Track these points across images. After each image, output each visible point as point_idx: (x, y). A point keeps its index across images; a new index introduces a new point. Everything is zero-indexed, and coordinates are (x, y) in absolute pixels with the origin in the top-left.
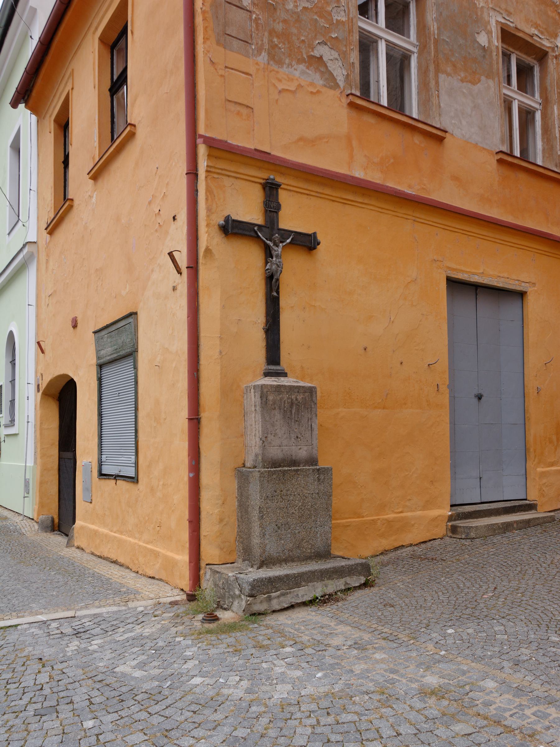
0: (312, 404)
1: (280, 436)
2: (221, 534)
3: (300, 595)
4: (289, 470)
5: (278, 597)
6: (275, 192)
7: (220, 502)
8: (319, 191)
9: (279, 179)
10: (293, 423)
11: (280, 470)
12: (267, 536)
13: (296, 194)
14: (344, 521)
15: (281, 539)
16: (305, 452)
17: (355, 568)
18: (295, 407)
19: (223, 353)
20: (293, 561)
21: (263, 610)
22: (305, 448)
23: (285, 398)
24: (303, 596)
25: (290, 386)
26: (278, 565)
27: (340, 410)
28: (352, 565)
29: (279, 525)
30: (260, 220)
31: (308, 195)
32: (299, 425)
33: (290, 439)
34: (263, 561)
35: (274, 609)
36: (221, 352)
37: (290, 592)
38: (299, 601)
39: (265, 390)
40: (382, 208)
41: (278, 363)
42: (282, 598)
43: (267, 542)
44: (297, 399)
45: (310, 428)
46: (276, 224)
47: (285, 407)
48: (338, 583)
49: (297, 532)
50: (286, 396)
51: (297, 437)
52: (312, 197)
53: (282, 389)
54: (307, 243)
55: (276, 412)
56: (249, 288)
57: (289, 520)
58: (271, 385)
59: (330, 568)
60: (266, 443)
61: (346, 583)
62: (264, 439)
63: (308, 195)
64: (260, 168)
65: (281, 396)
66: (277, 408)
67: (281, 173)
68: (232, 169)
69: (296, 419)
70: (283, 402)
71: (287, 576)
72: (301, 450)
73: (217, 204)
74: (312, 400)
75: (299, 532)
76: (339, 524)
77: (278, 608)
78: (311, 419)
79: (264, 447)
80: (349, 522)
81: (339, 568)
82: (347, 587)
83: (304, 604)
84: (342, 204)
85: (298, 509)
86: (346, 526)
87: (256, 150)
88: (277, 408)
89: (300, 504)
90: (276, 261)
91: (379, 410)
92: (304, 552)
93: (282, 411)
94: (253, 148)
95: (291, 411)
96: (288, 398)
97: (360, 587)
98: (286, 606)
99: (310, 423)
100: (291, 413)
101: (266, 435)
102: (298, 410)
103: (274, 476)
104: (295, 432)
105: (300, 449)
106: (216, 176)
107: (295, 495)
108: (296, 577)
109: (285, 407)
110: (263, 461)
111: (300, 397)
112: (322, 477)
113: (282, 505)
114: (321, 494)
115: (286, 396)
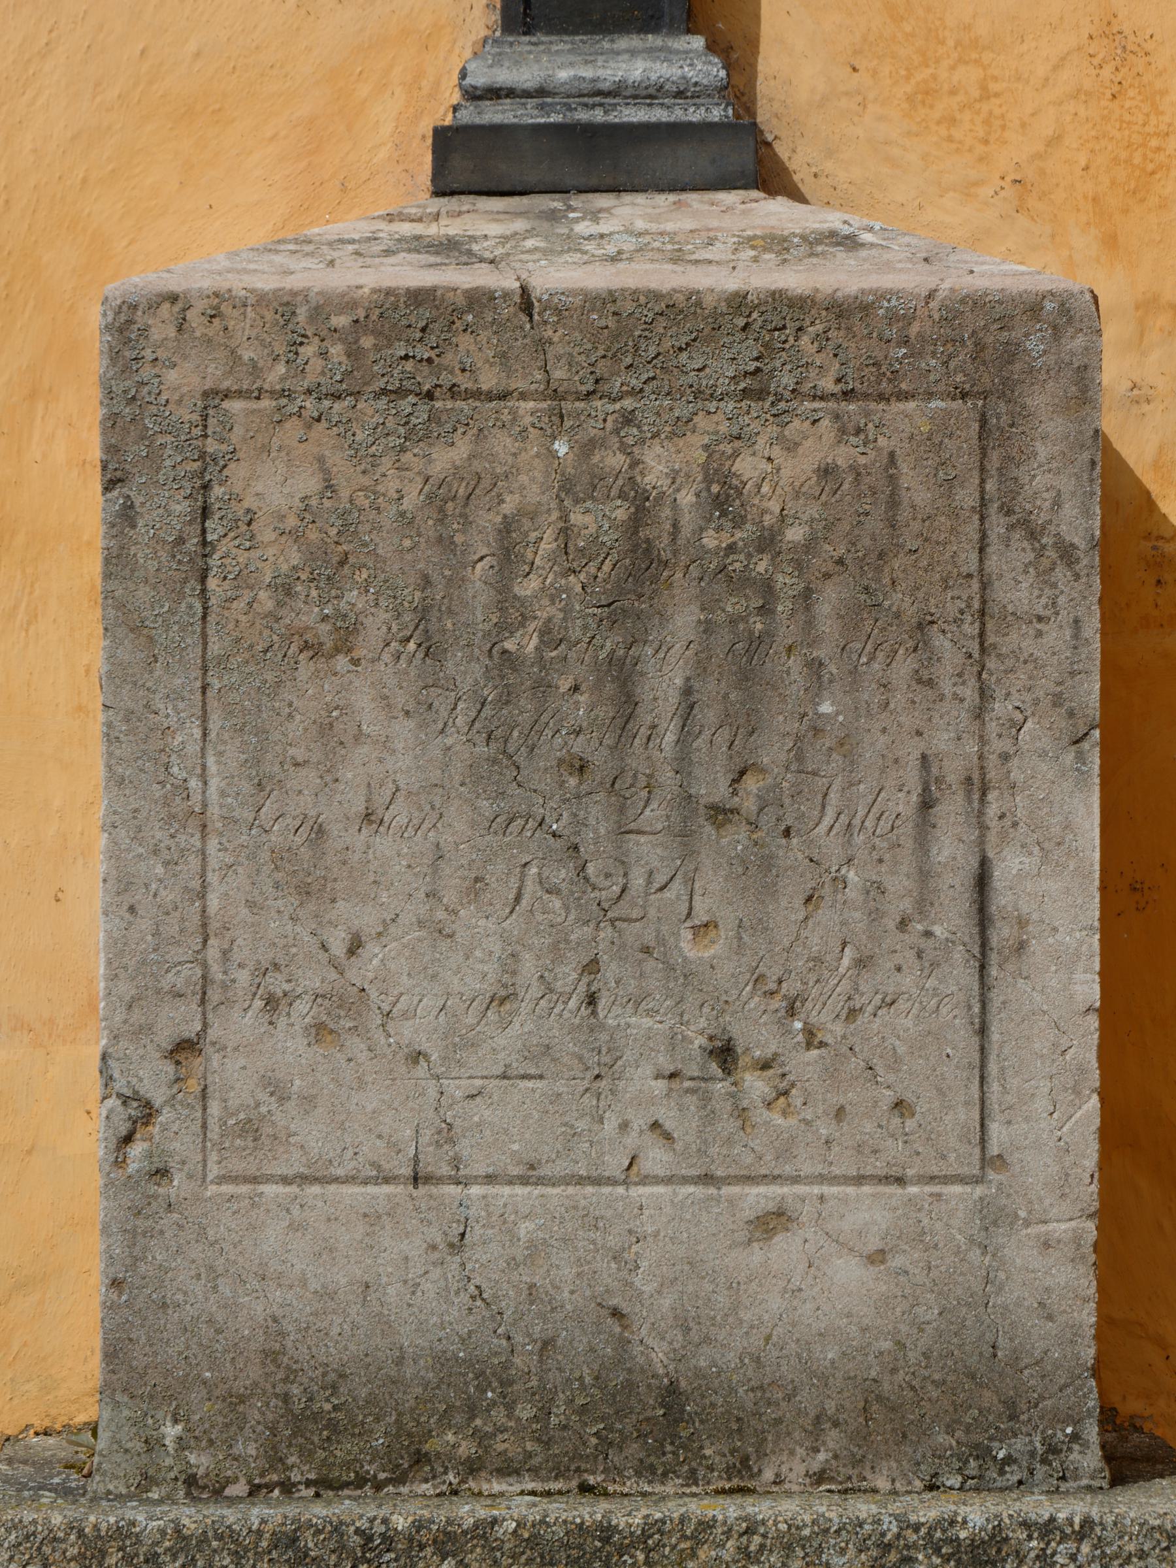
10: (650, 853)
16: (848, 1272)
18: (684, 619)
22: (869, 1212)
23: (530, 489)
25: (610, 298)
32: (758, 872)
33: (603, 1073)
39: (183, 380)
44: (724, 499)
45: (951, 919)
47: (509, 612)
50: (526, 462)
51: (724, 1053)
53: (476, 357)
55: (370, 690)
60: (174, 1133)
62: (152, 1077)
65: (445, 458)
69: (712, 786)
70: (481, 542)
72: (786, 1250)
78: (978, 786)
93: (466, 670)
95: (622, 677)
96: (569, 489)
99: (951, 849)
100: (627, 705)
101: (181, 1019)
102: (746, 661)
104: (688, 975)
105: (774, 1221)
109: (509, 612)
110: (125, 1365)
111: (782, 465)
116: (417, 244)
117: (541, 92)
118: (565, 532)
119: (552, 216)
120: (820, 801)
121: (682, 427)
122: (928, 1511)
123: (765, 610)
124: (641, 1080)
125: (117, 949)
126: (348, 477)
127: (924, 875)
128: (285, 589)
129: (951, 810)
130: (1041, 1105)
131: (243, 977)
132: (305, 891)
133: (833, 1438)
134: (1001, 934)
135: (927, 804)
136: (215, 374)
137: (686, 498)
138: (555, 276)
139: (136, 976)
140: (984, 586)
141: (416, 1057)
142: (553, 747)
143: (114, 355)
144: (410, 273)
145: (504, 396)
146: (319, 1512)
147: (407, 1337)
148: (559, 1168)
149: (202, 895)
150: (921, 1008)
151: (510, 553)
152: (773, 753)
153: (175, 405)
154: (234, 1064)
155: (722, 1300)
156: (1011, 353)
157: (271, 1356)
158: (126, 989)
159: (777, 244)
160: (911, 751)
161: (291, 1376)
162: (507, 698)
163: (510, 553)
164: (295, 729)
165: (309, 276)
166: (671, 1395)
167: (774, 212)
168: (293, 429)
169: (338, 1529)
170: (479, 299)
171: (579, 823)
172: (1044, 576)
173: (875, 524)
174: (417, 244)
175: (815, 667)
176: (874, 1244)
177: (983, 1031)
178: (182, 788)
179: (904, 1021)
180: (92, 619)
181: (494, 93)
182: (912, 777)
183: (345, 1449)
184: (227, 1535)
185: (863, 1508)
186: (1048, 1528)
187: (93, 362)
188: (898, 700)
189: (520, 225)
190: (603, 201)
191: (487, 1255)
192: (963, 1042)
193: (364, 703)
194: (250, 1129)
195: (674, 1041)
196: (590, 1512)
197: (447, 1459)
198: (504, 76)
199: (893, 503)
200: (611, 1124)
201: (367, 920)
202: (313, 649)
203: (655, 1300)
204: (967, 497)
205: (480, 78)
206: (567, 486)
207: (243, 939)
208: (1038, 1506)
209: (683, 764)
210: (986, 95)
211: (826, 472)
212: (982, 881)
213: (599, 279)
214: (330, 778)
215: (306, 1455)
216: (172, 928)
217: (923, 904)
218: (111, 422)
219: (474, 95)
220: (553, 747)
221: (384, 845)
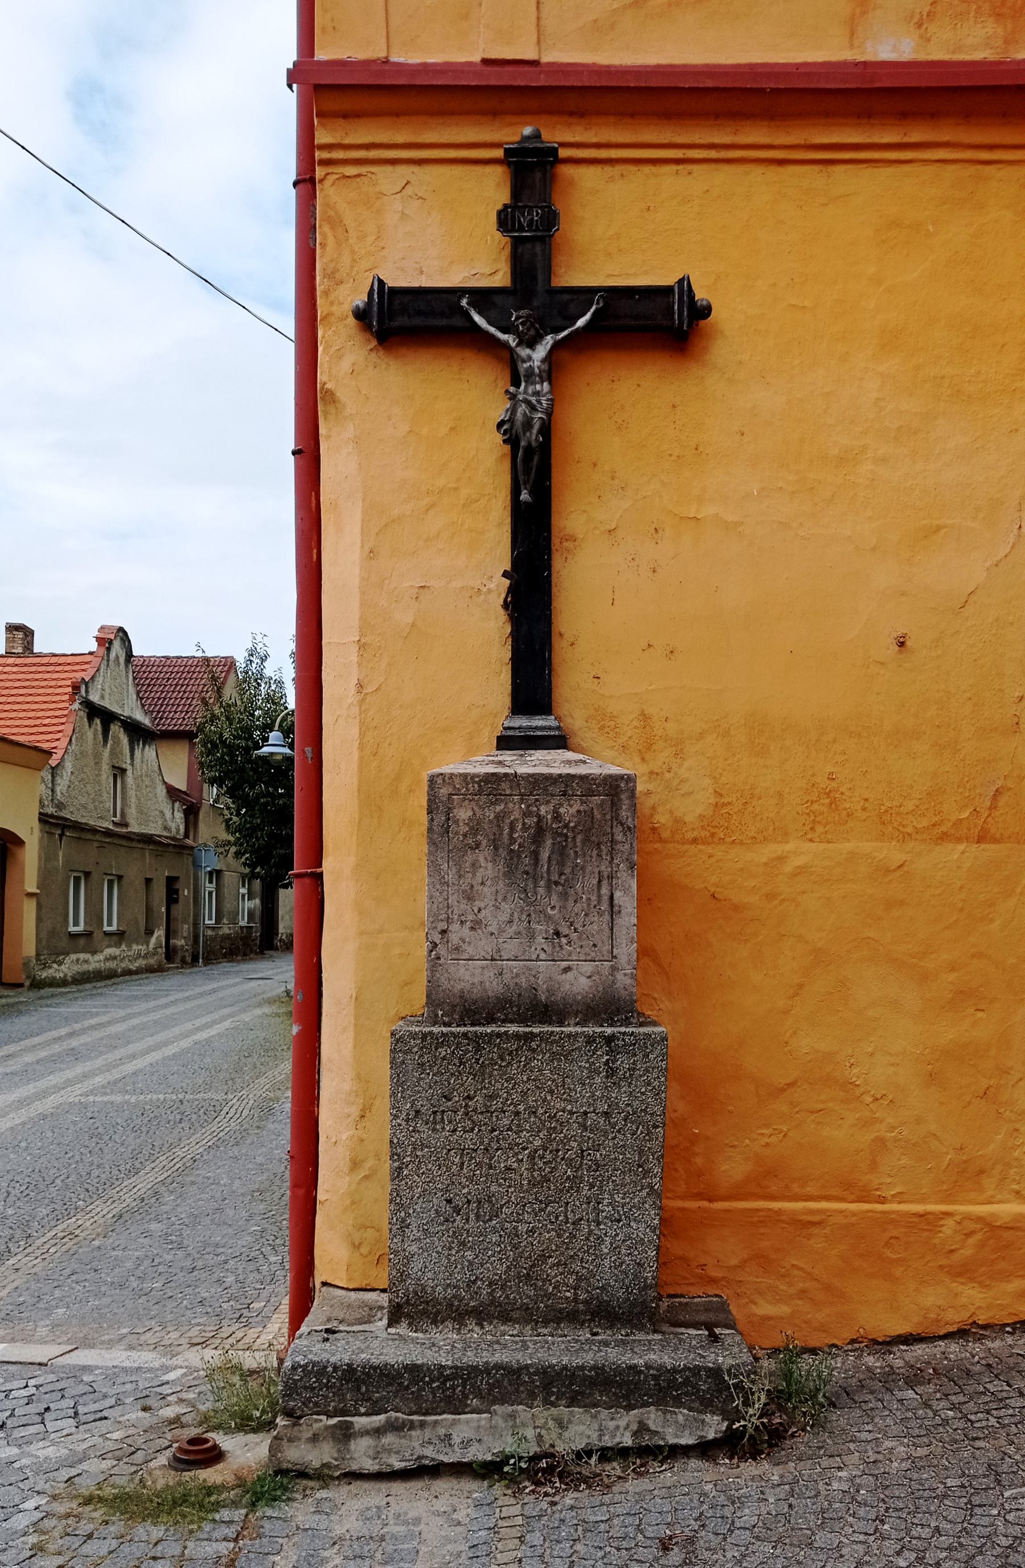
0: (618, 829)
1: (493, 928)
2: (353, 1203)
3: (456, 1440)
4: (499, 1035)
5: (378, 1432)
6: (538, 175)
7: (355, 1111)
8: (716, 140)
9: (555, 134)
10: (541, 891)
11: (465, 1035)
12: (413, 1232)
13: (632, 168)
14: (799, 1205)
15: (463, 1244)
17: (686, 1382)
18: (549, 842)
19: (369, 689)
20: (506, 1318)
21: (316, 1464)
22: (588, 967)
23: (516, 814)
24: (466, 1444)
25: (532, 775)
26: (449, 1324)
27: (790, 846)
28: (675, 1370)
29: (459, 1201)
30: (500, 274)
31: (678, 161)
32: (564, 896)
33: (532, 937)
34: (399, 1306)
35: (354, 1467)
36: (360, 686)
37: (422, 1425)
38: (446, 1459)
39: (444, 791)
40: (991, 147)
41: (544, 707)
42: (388, 1439)
43: (414, 1248)
44: (557, 817)
45: (605, 906)
46: (540, 278)
47: (512, 841)
48: (612, 1424)
49: (522, 1228)
51: (557, 934)
52: (695, 168)
54: (663, 323)
55: (483, 856)
56: (456, 489)
57: (494, 1188)
58: (465, 776)
59: (582, 1368)
60: (442, 950)
61: (642, 1428)
63: (678, 161)
64: (494, 114)
65: (498, 808)
66: (484, 842)
67: (571, 114)
68: (400, 138)
69: (555, 877)
71: (414, 1369)
72: (570, 975)
73: (353, 252)
74: (616, 817)
75: (532, 1231)
76: (779, 1212)
77: (370, 1466)
78: (611, 877)
79: (435, 962)
80: (820, 1211)
81: (618, 1370)
82: (646, 1440)
83: (460, 1470)
84: (816, 168)
85: (531, 1157)
86: (805, 1225)
87: (486, 62)
88: (484, 842)
89: (538, 1143)
90: (525, 392)
91: (961, 847)
92: (548, 1296)
94: (476, 58)
95: (536, 856)
96: (526, 814)
97: (705, 1450)
98: (398, 1465)
99: (605, 891)
101: (442, 926)
102: (561, 853)
103: (442, 1052)
104: (549, 918)
105: (567, 970)
106: (351, 170)
107: (517, 1113)
108: (448, 1378)
109: (512, 841)
110: (431, 1000)
112: (623, 1063)
113: (470, 1140)
114: (617, 1118)
115: (516, 809)
116: (493, 762)
117: (519, 728)
118: (524, 824)
119: (522, 755)
120: (72, 1475)
121: (548, 802)
122: (599, 1030)
123: (566, 841)
124: (540, 939)
125: (430, 910)
126: (479, 812)
127: (599, 896)
128: (465, 835)
129: (605, 882)
130: (624, 945)
131: (456, 917)
132: (469, 899)
133: (580, 1015)
134: (616, 909)
135: (600, 881)
136: (451, 790)
137: (549, 817)
138: (522, 770)
139: (434, 917)
140: (612, 835)
141: (492, 934)
142: (521, 868)
143: (430, 786)
144: (491, 769)
145: (511, 795)
146: (471, 1029)
147: (490, 994)
148: (523, 958)
149: (447, 899)
150: (598, 925)
151: (512, 828)
152: (567, 871)
153: (442, 796)
154: (454, 935)
155: (557, 986)
156: (618, 786)
157: (461, 997)
158: (431, 919)
159: (569, 762)
160: (597, 870)
161: (466, 1001)
162: (511, 859)
163: (512, 828)
164: (467, 864)
165: (470, 770)
166: (546, 1006)
167: (570, 755)
168: (467, 802)
169: (476, 1032)
170: (506, 775)
171: (526, 885)
172: (625, 834)
173: (589, 822)
174: (493, 762)
175: (576, 852)
176: (589, 974)
177: (612, 929)
178: (444, 877)
179: (595, 927)
180: (424, 840)
181: (509, 728)
182: (597, 875)
183: (477, 1017)
184: (452, 1033)
185: (585, 1029)
186: (624, 1033)
187: (426, 788)
188: (594, 859)
189: (515, 758)
190: (532, 752)
191: (507, 976)
192: (607, 931)
193: (482, 859)
194: (457, 949)
195: (546, 931)
196: (528, 1029)
197: (499, 1019)
198: (512, 725)
199: (593, 818)
200: (533, 948)
201: (482, 905)
202: (471, 848)
203: (542, 985)
204: (608, 817)
205: (507, 724)
206: (524, 814)
207: (456, 909)
208: (623, 1029)
209: (548, 872)
210: (616, 727)
211: (579, 811)
212: (612, 897)
213: (531, 770)
214: (474, 874)
215: (469, 1018)
216: (441, 906)
217: (599, 902)
218: (429, 800)
219: (505, 728)
220: (521, 868)
221: (486, 889)
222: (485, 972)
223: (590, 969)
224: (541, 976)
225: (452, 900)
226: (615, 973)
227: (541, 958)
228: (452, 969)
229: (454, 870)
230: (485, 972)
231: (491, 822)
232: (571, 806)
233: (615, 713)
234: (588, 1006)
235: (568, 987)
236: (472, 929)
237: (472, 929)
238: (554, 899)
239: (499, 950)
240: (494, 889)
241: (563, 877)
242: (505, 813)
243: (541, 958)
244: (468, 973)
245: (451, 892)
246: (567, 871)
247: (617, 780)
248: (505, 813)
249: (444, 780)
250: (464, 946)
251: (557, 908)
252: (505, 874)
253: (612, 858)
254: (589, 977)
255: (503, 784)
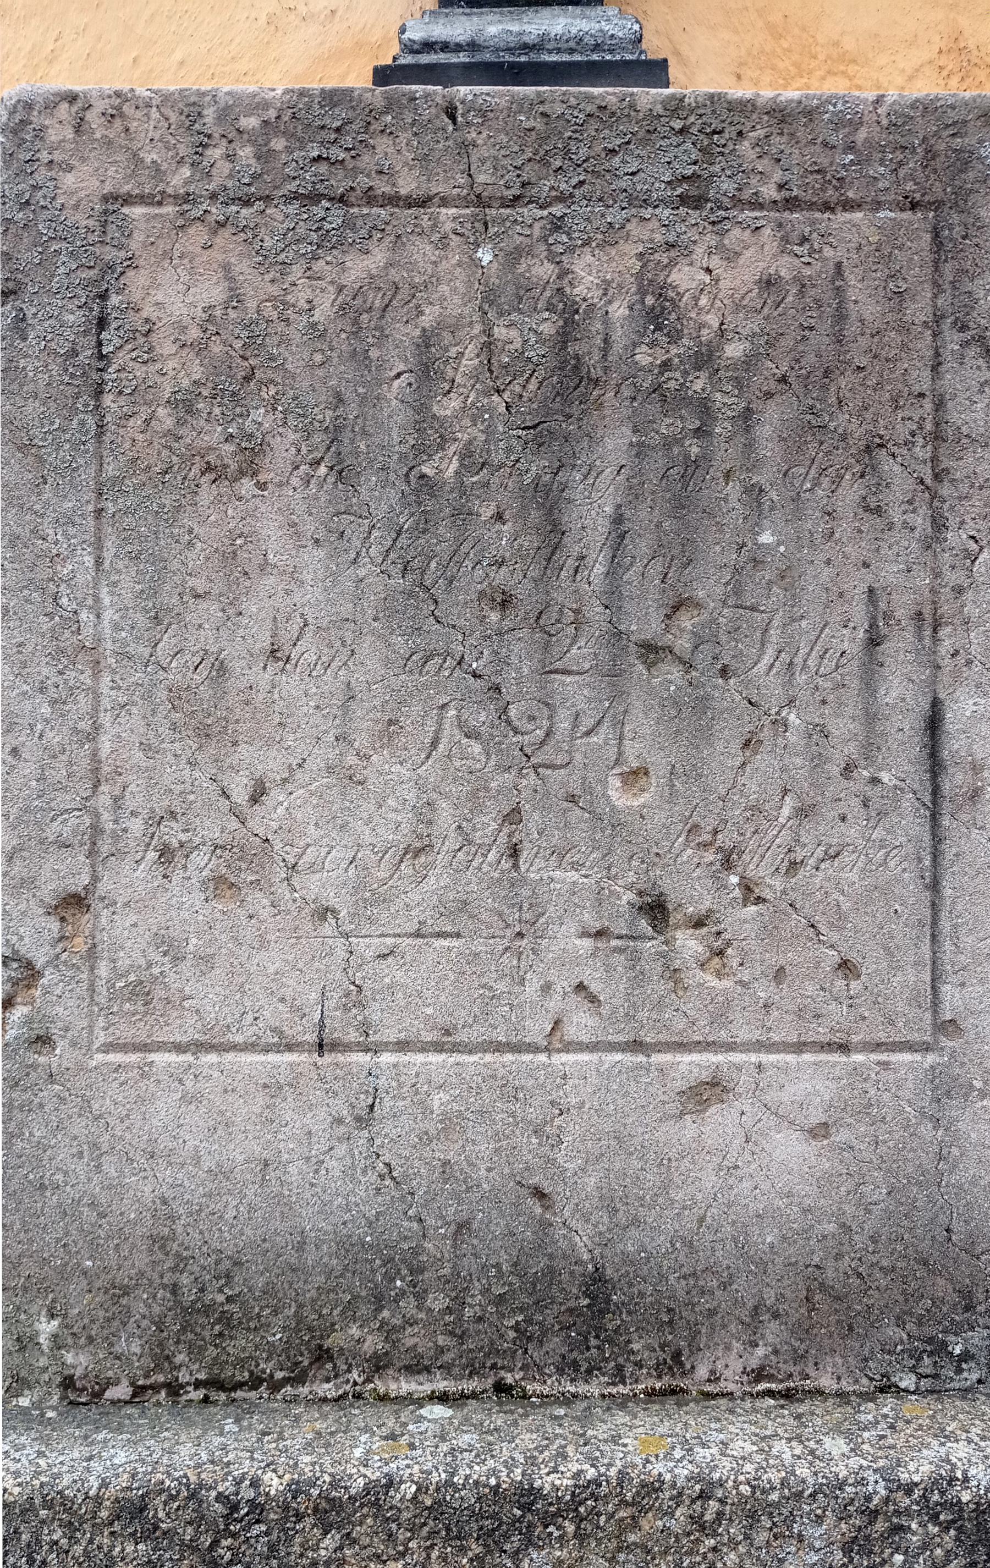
10: (576, 693)
18: (615, 442)
22: (810, 1082)
23: (451, 299)
33: (525, 931)
39: (82, 183)
44: (659, 313)
45: (900, 765)
47: (428, 434)
51: (656, 910)
55: (276, 513)
60: (60, 999)
65: (359, 267)
69: (645, 621)
72: (721, 1122)
78: (929, 622)
88: (284, 446)
95: (547, 509)
101: (70, 872)
105: (707, 1092)
118: (488, 347)
121: (611, 235)
124: (567, 939)
126: (258, 288)
127: (871, 717)
128: (184, 405)
131: (136, 826)
132: (204, 733)
133: (772, 1331)
134: (955, 780)
135: (874, 641)
136: (116, 178)
137: (619, 311)
140: (939, 405)
141: (324, 913)
145: (423, 202)
149: (93, 735)
151: (428, 370)
155: (652, 1178)
157: (159, 1242)
160: (857, 584)
161: (180, 1264)
162: (425, 525)
163: (428, 370)
164: (195, 557)
166: (596, 1283)
168: (198, 234)
171: (501, 662)
173: (821, 340)
175: (755, 493)
176: (817, 1117)
177: (935, 886)
181: (428, 46)
182: (859, 613)
183: (239, 1344)
188: (844, 529)
191: (397, 1128)
192: (912, 892)
193: (271, 530)
194: (140, 992)
199: (841, 316)
201: (272, 764)
203: (581, 1182)
204: (918, 310)
206: (490, 297)
209: (612, 598)
211: (768, 283)
212: (934, 723)
214: (233, 610)
215: (196, 1351)
217: (870, 747)
221: (291, 684)
222: (287, 1110)
223: (825, 1089)
224: (573, 1130)
225: (118, 738)
226: (953, 1108)
227: (571, 1032)
228: (111, 1098)
229: (128, 583)
230: (287, 1110)
231: (316, 332)
232: (731, 257)
233: (849, 44)
234: (815, 1289)
235: (709, 1180)
236: (220, 885)
237: (220, 885)
238: (644, 738)
239: (356, 996)
240: (331, 682)
241: (686, 621)
242: (398, 295)
243: (571, 1032)
244: (195, 1117)
245: (108, 695)
246: (708, 587)
247: (958, 129)
248: (398, 295)
249: (79, 126)
250: (179, 979)
251: (656, 781)
252: (388, 610)
253: (939, 524)
254: (820, 1131)
255: (383, 144)
